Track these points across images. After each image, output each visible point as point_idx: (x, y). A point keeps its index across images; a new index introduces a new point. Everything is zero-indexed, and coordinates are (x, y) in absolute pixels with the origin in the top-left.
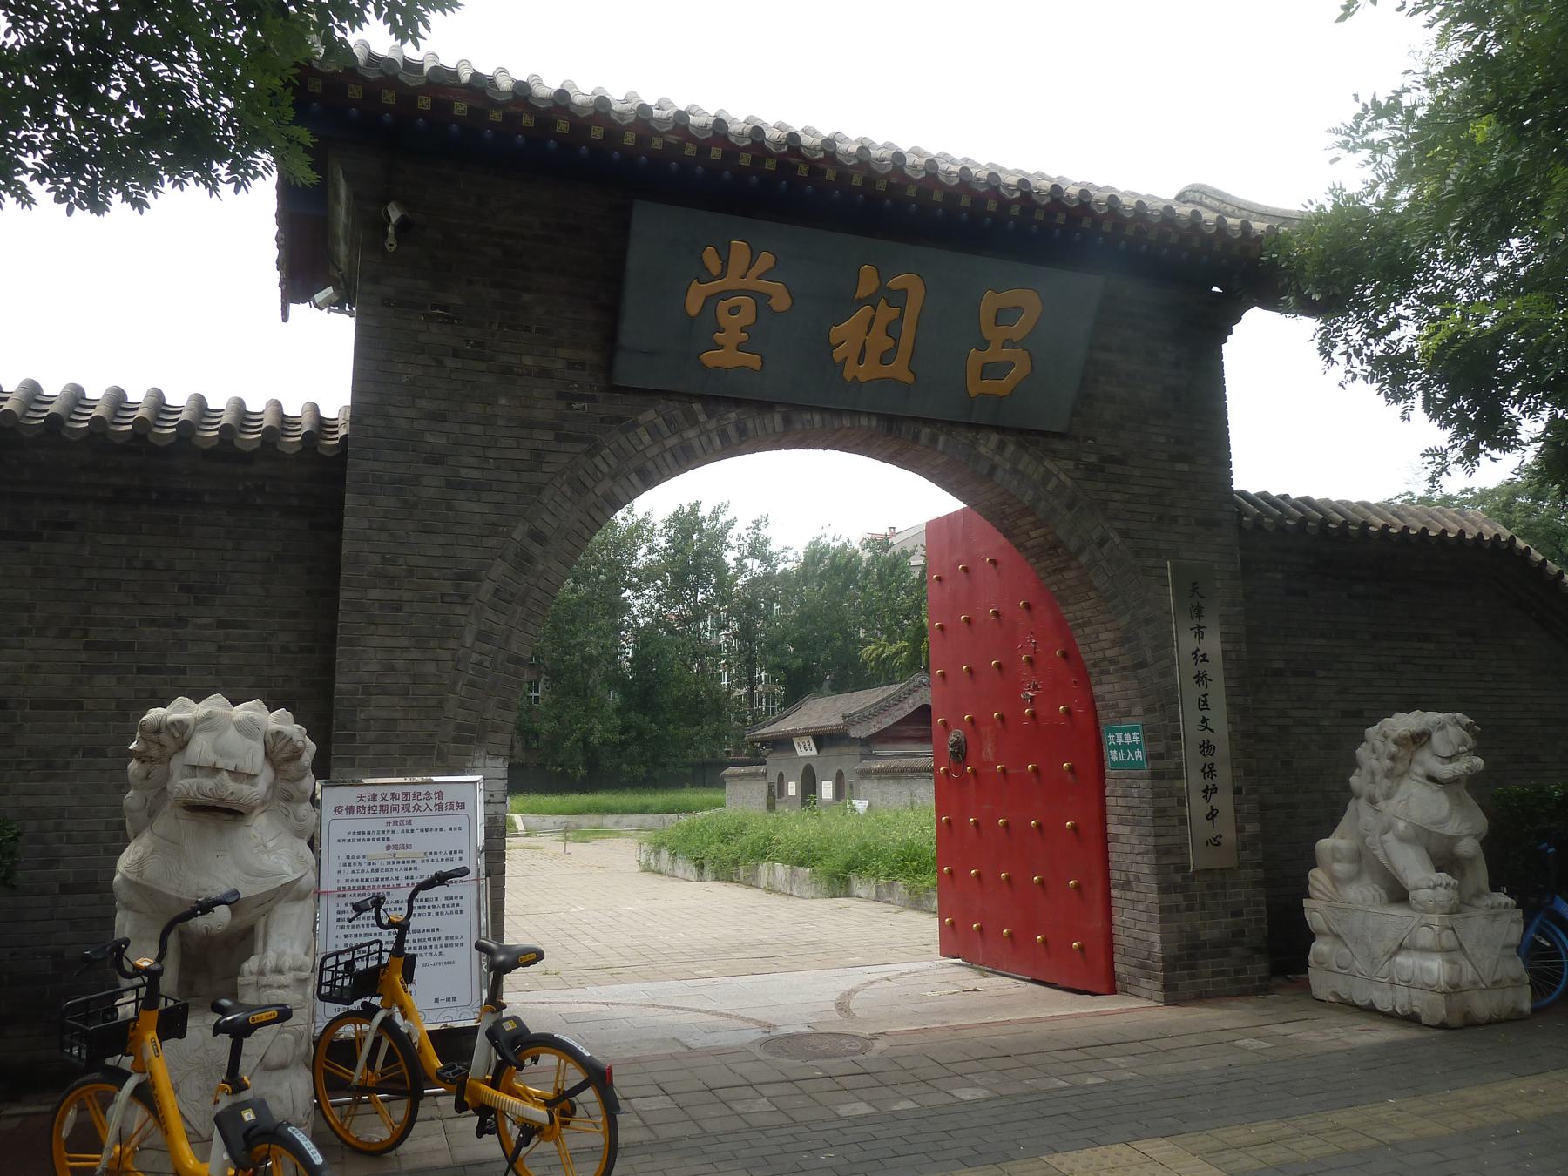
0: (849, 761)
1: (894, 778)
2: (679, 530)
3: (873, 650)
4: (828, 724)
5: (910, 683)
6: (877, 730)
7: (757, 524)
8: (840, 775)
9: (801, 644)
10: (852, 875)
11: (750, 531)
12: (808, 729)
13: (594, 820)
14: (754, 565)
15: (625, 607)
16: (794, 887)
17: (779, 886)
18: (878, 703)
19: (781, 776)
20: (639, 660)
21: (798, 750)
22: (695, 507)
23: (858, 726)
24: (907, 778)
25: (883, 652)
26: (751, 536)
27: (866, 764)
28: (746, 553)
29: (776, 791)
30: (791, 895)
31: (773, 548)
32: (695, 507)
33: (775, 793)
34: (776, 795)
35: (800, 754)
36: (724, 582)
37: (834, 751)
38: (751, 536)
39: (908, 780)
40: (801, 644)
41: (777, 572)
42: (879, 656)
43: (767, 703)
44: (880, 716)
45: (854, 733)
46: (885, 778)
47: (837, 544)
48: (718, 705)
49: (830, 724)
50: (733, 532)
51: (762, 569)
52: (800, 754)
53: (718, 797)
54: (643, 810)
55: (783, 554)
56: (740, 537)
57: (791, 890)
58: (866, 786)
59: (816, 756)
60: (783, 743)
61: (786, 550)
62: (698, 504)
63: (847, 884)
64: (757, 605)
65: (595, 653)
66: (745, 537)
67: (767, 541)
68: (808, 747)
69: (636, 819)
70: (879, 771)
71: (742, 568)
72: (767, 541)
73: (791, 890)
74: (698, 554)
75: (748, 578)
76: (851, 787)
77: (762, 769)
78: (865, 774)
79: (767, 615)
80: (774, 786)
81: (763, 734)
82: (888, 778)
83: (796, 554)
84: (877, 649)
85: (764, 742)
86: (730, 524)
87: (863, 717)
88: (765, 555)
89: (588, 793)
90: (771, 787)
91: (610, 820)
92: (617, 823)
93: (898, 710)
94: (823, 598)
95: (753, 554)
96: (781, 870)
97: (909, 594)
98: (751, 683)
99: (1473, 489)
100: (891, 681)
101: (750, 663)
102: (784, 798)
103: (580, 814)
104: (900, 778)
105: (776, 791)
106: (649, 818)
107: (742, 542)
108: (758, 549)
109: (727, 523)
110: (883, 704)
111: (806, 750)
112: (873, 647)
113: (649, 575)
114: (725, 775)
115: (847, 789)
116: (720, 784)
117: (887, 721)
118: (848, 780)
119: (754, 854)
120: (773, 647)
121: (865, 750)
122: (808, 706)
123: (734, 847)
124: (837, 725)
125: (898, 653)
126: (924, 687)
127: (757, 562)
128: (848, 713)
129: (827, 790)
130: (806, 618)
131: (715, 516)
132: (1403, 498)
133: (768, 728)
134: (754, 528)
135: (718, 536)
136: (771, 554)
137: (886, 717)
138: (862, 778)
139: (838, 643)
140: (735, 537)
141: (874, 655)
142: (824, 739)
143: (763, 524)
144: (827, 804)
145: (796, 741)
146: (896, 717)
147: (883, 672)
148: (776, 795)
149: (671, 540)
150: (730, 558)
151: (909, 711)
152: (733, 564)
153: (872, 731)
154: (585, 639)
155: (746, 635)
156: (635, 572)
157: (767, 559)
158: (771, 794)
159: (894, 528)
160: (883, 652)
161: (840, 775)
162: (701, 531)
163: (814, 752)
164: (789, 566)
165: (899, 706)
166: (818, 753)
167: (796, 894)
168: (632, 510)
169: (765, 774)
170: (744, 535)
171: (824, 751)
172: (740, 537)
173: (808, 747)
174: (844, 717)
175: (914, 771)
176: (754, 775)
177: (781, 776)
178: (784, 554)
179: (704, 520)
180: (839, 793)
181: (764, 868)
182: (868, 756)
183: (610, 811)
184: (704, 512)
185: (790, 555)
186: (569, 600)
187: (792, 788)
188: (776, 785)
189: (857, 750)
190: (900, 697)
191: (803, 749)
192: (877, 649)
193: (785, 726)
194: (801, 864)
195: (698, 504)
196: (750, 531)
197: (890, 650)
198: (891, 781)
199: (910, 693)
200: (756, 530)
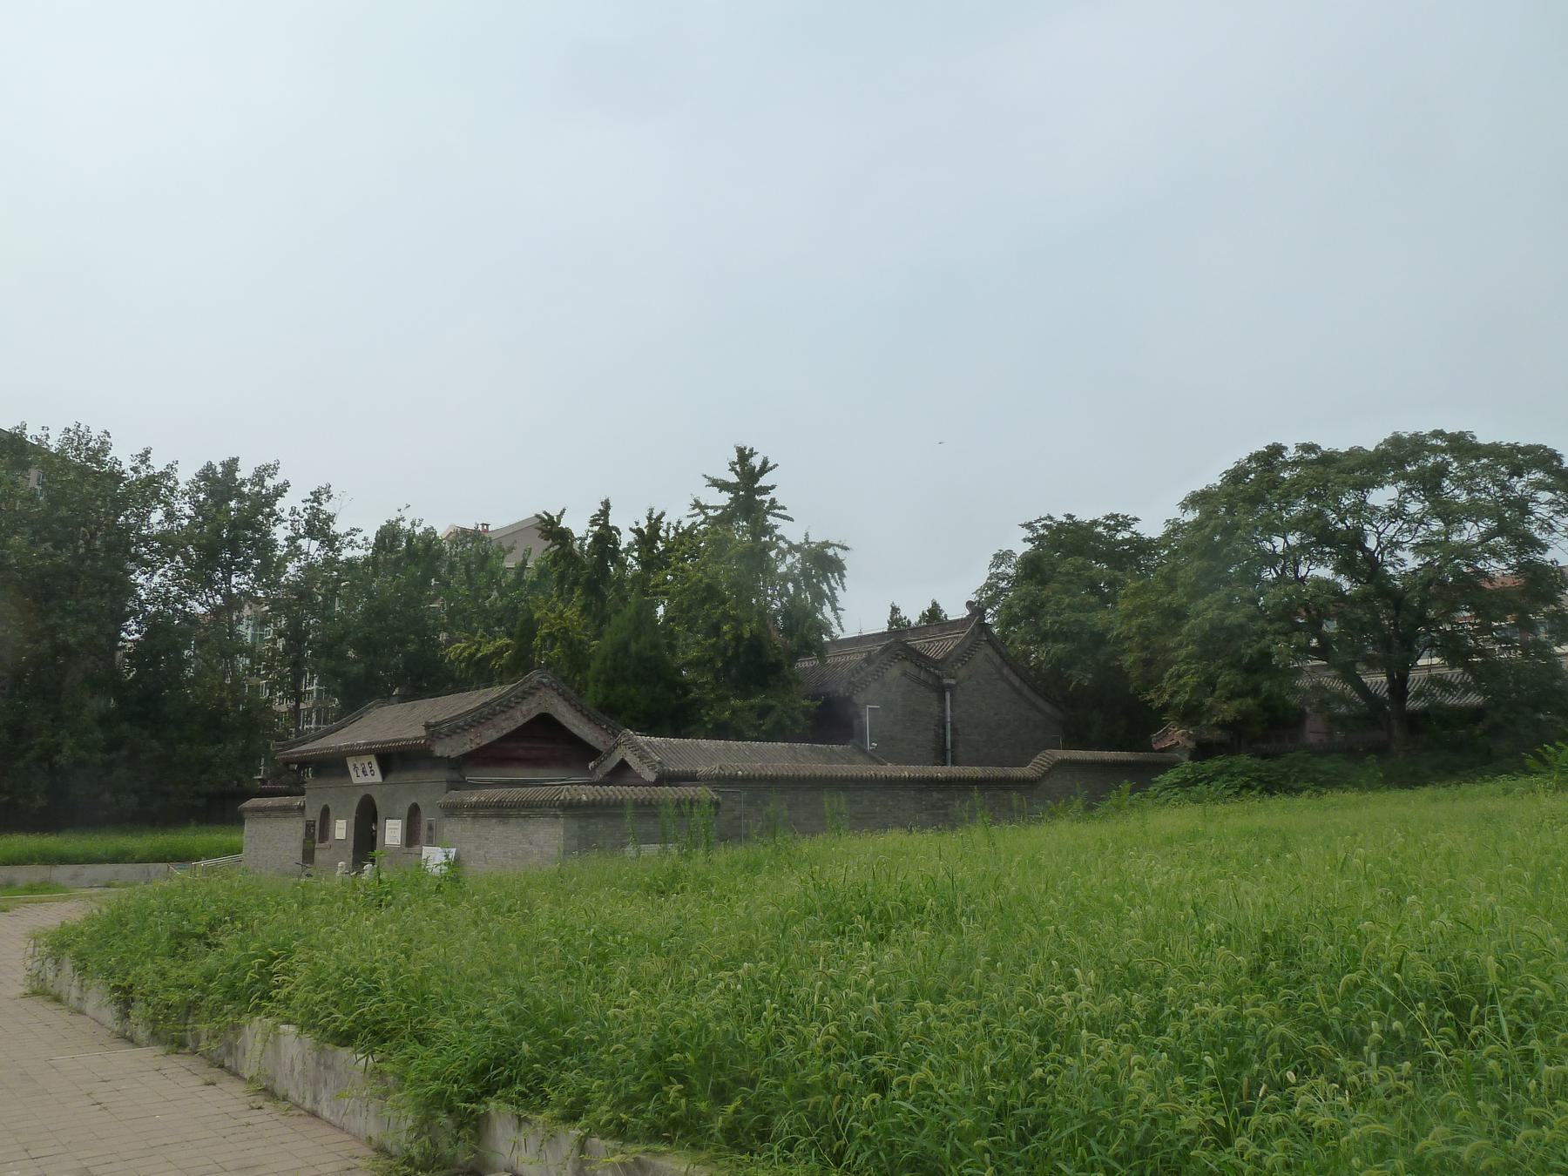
0: (429, 791)
1: (498, 816)
2: (210, 494)
3: (465, 649)
4: (401, 737)
5: (524, 683)
6: (474, 746)
7: (316, 497)
8: (414, 811)
9: (367, 647)
10: (499, 1111)
11: (308, 505)
12: (370, 744)
13: (37, 873)
14: (311, 546)
15: (131, 590)
16: (324, 1095)
17: (284, 1085)
18: (477, 709)
19: (325, 812)
20: (141, 654)
21: (353, 774)
22: (231, 466)
23: (447, 740)
24: (519, 816)
25: (478, 650)
26: (308, 511)
27: (455, 796)
28: (302, 531)
29: (317, 832)
30: (314, 1114)
31: (338, 528)
32: (231, 466)
33: (318, 831)
34: (317, 837)
35: (356, 781)
36: (269, 569)
37: (408, 776)
38: (308, 511)
39: (521, 820)
40: (367, 647)
41: (341, 558)
42: (472, 655)
43: (318, 722)
44: (481, 728)
45: (440, 750)
46: (484, 816)
47: (419, 531)
48: (254, 721)
49: (405, 736)
50: (282, 504)
51: (322, 553)
52: (356, 781)
53: (235, 838)
54: (118, 858)
55: (349, 537)
56: (294, 512)
57: (315, 1100)
58: (451, 827)
59: (381, 784)
60: (332, 766)
61: (354, 533)
62: (235, 461)
63: (476, 1128)
64: (311, 596)
65: (71, 640)
66: (301, 512)
67: (330, 518)
68: (368, 770)
69: (106, 870)
70: (475, 807)
71: (295, 551)
72: (330, 518)
73: (315, 1100)
74: (234, 526)
75: (303, 563)
76: (430, 828)
77: (298, 801)
78: (452, 811)
79: (324, 612)
80: (314, 826)
81: (304, 752)
82: (491, 816)
83: (365, 539)
84: (469, 647)
85: (303, 763)
86: (280, 491)
87: (456, 727)
88: (326, 535)
89: (1361, 788)
90: (309, 826)
91: (62, 873)
92: (75, 876)
93: (507, 719)
94: (397, 591)
95: (311, 533)
96: (294, 1045)
97: (502, 595)
98: (298, 696)
99: (1117, 515)
100: (489, 683)
101: (297, 665)
102: (327, 843)
103: (14, 864)
104: (508, 816)
105: (317, 832)
106: (126, 870)
107: (297, 517)
108: (318, 526)
109: (276, 488)
110: (486, 710)
111: (365, 774)
112: (463, 645)
113: (169, 544)
114: (246, 809)
115: (424, 832)
116: (237, 821)
117: (489, 735)
118: (426, 818)
119: (234, 994)
120: (329, 648)
121: (455, 776)
122: (372, 715)
123: (192, 972)
124: (416, 739)
125: (498, 653)
126: (543, 689)
127: (315, 544)
128: (433, 721)
129: (392, 832)
130: (377, 613)
131: (260, 476)
132: (1044, 522)
133: (313, 744)
134: (314, 502)
135: (265, 502)
136: (336, 537)
137: (488, 729)
138: (446, 816)
139: (412, 648)
140: (288, 510)
141: (466, 654)
142: (391, 759)
143: (324, 497)
144: (393, 853)
145: (351, 762)
146: (502, 730)
147: (480, 672)
148: (317, 837)
149: (198, 507)
150: (280, 534)
151: (521, 721)
152: (281, 542)
153: (468, 748)
154: (59, 622)
155: (295, 636)
156: (146, 540)
157: (329, 541)
158: (309, 834)
159: (487, 525)
160: (478, 650)
161: (414, 811)
162: (241, 497)
163: (378, 778)
164: (359, 553)
165: (508, 715)
166: (384, 778)
167: (326, 1114)
168: (147, 459)
169: (302, 809)
170: (300, 508)
171: (391, 778)
172: (294, 512)
173: (368, 770)
174: (427, 726)
175: (532, 807)
176: (286, 810)
177: (325, 812)
178: (352, 537)
179: (243, 483)
180: (412, 837)
181: (255, 1030)
182: (454, 785)
183: (64, 860)
184: (244, 472)
185: (359, 538)
186: (38, 567)
187: (341, 829)
188: (317, 825)
189: (443, 775)
190: (510, 701)
191: (360, 773)
192: (469, 647)
193: (337, 741)
194: (345, 1039)
195: (235, 461)
196: (308, 505)
197: (487, 649)
198: (494, 821)
199: (525, 695)
200: (315, 504)
